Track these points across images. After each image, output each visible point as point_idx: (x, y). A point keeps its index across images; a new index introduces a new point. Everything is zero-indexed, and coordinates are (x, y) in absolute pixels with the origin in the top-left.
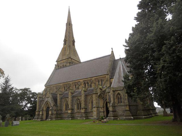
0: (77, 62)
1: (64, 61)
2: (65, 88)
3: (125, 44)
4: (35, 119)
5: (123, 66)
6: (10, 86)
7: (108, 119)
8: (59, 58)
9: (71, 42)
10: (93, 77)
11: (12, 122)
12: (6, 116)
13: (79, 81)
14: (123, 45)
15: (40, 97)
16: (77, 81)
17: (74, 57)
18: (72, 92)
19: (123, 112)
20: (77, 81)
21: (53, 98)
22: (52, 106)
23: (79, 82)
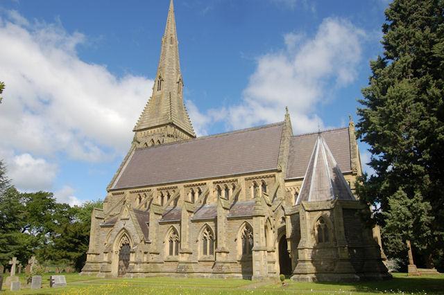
0: (186, 136)
1: (156, 129)
2: (140, 199)
3: (363, 98)
4: (86, 273)
5: (326, 151)
6: (7, 184)
7: (294, 279)
8: (141, 122)
9: (175, 84)
10: (239, 175)
11: (49, 278)
12: (29, 262)
13: (204, 182)
14: (359, 101)
15: (97, 218)
16: (197, 183)
17: (181, 122)
18: (226, 207)
19: (331, 263)
20: (197, 183)
21: (139, 221)
22: (139, 242)
23: (202, 184)
